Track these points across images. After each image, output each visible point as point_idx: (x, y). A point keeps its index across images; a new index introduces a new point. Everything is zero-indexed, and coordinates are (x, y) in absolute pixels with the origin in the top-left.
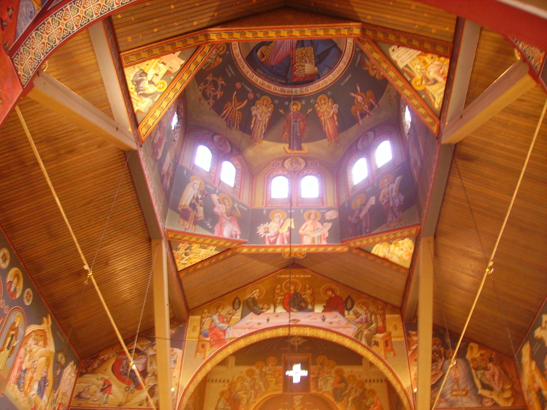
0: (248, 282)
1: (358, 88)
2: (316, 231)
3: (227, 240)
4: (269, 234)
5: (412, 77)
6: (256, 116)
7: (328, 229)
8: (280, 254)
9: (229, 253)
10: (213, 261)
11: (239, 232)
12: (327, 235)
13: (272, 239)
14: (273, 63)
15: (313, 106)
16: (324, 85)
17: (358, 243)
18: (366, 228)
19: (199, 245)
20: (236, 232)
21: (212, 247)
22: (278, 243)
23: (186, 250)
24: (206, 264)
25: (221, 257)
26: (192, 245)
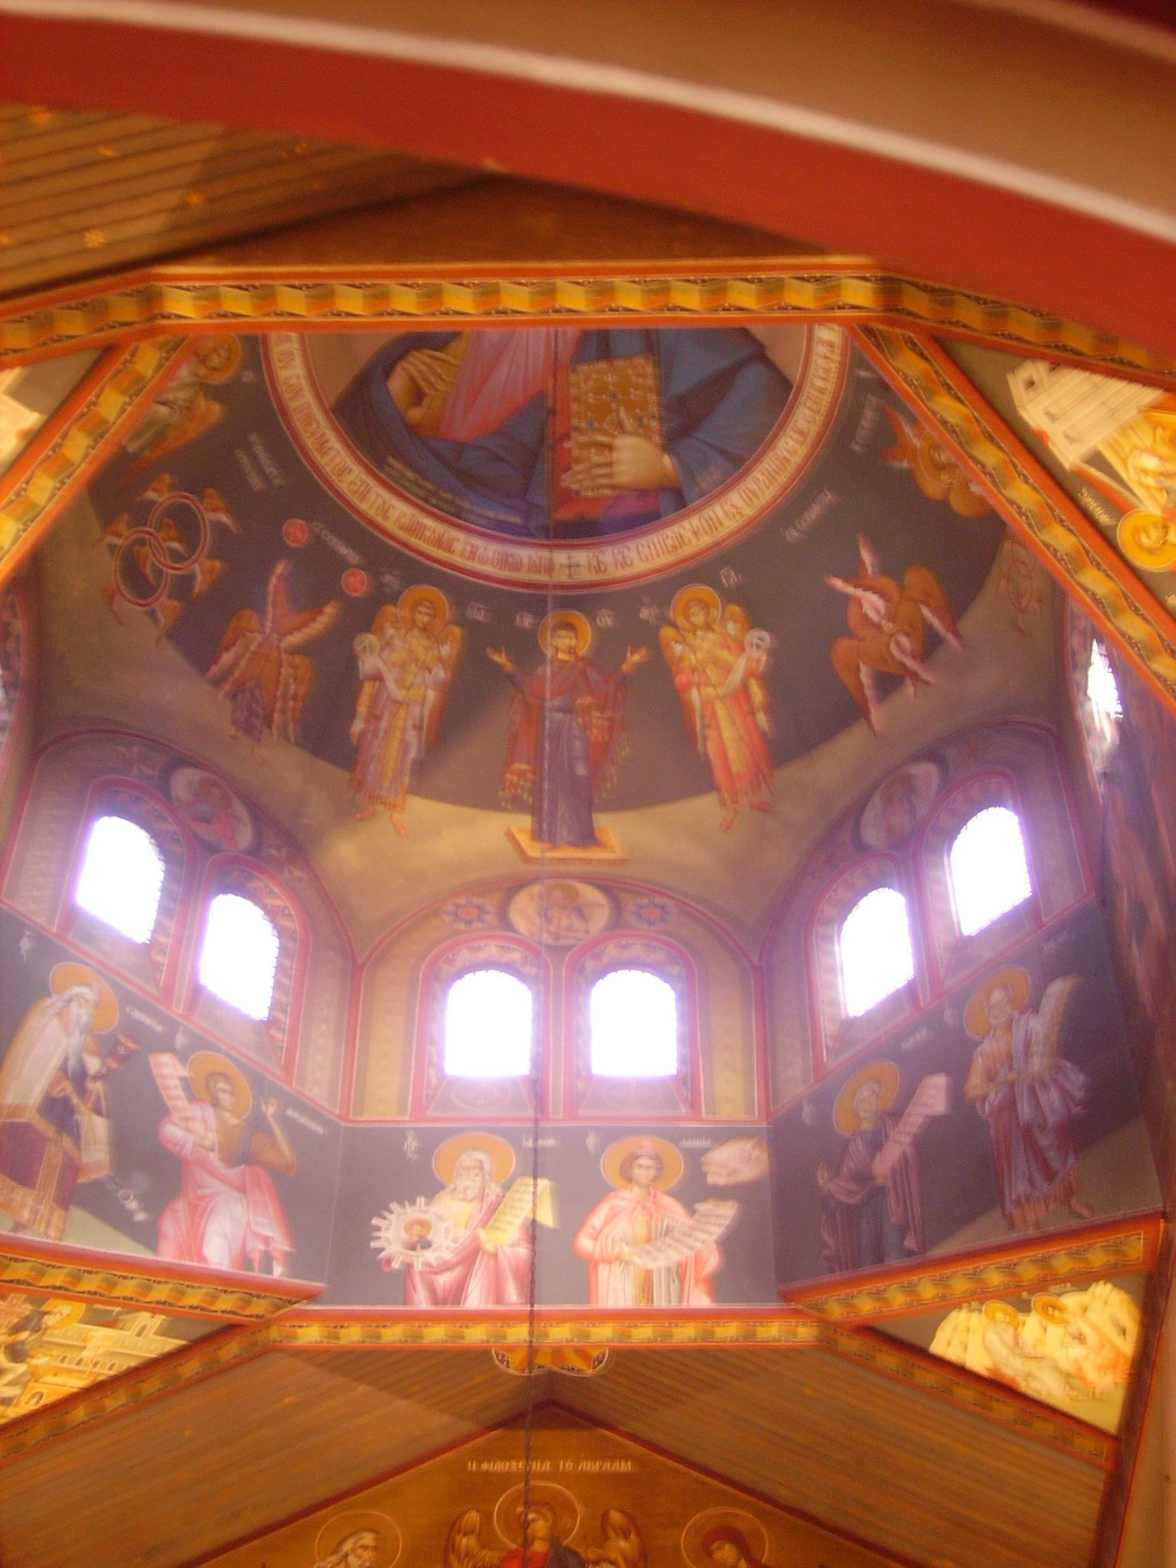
0: (323, 1491)
1: (867, 557)
2: (659, 1243)
3: (222, 1282)
4: (430, 1256)
5: (1120, 508)
6: (378, 678)
7: (718, 1231)
8: (480, 1356)
9: (231, 1349)
10: (151, 1385)
11: (281, 1244)
12: (713, 1261)
13: (443, 1280)
14: (461, 432)
15: (649, 637)
16: (706, 540)
17: (866, 1306)
18: (903, 1230)
19: (80, 1308)
20: (266, 1240)
21: (144, 1318)
22: (475, 1299)
23: (17, 1329)
24: (114, 1402)
25: (191, 1367)
26: (43, 1309)
